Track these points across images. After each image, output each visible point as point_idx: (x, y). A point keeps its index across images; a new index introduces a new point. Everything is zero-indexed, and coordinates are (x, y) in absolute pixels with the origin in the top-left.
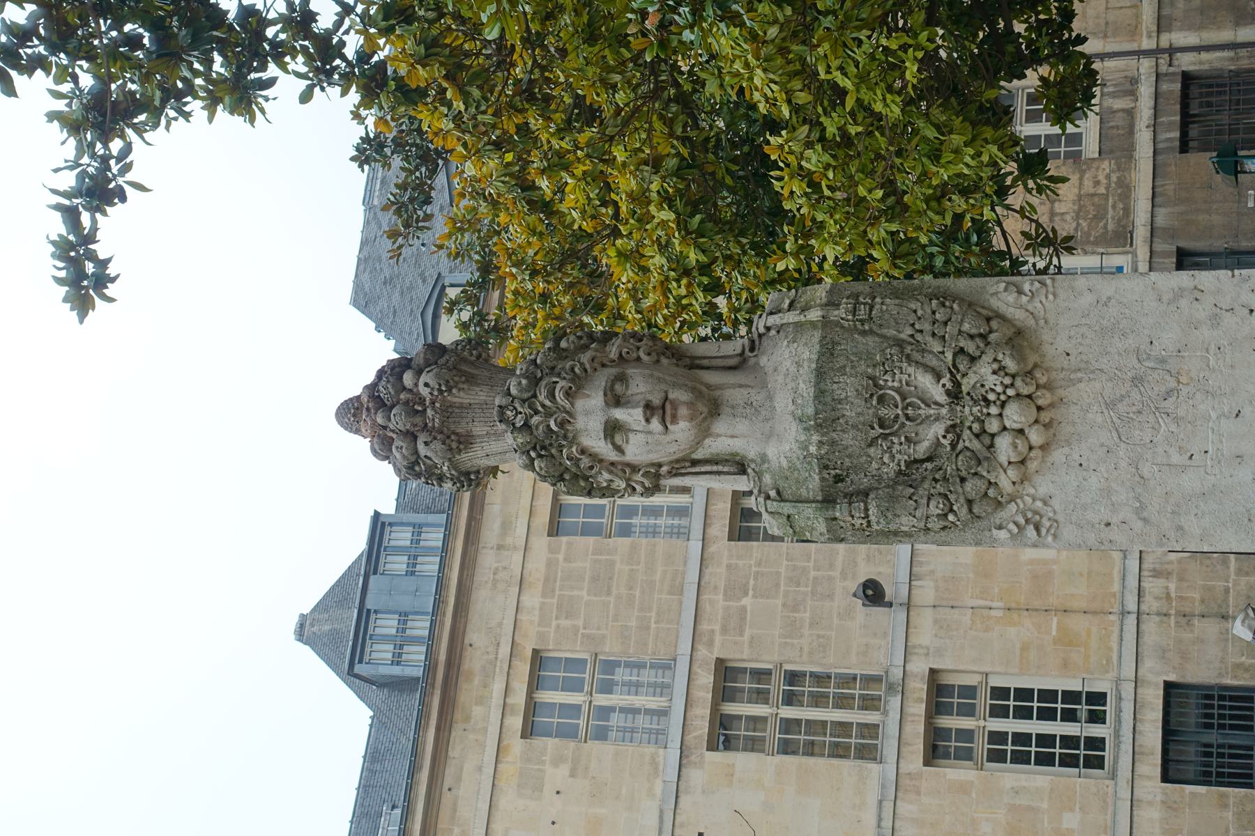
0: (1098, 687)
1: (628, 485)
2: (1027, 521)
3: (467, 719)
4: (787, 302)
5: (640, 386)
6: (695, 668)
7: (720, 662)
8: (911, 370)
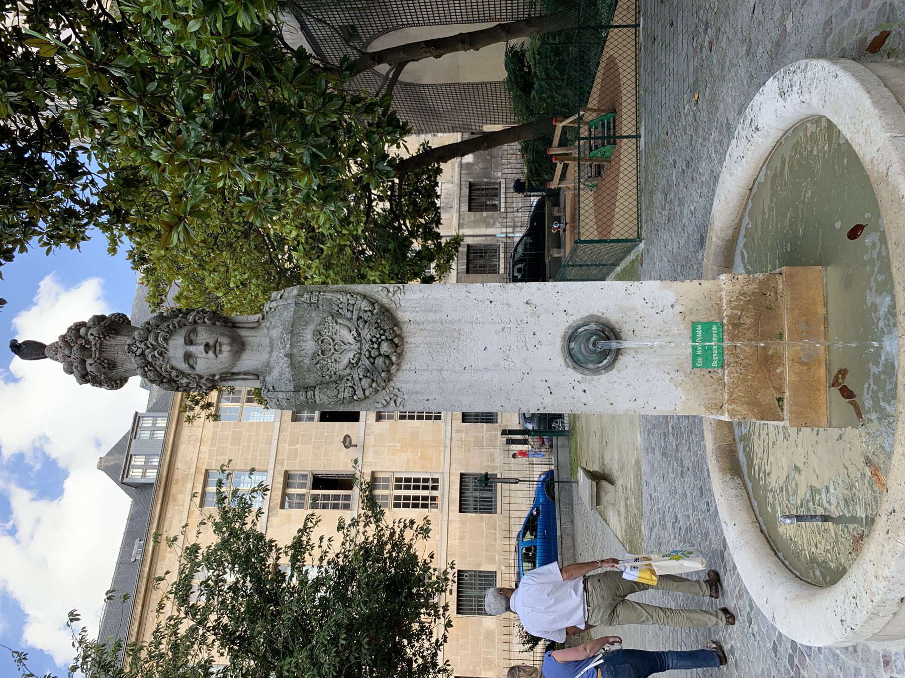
0: (435, 476)
1: (198, 385)
2: (391, 399)
3: (175, 500)
4: (280, 295)
5: (204, 336)
6: (275, 475)
7: (286, 472)
8: (337, 327)
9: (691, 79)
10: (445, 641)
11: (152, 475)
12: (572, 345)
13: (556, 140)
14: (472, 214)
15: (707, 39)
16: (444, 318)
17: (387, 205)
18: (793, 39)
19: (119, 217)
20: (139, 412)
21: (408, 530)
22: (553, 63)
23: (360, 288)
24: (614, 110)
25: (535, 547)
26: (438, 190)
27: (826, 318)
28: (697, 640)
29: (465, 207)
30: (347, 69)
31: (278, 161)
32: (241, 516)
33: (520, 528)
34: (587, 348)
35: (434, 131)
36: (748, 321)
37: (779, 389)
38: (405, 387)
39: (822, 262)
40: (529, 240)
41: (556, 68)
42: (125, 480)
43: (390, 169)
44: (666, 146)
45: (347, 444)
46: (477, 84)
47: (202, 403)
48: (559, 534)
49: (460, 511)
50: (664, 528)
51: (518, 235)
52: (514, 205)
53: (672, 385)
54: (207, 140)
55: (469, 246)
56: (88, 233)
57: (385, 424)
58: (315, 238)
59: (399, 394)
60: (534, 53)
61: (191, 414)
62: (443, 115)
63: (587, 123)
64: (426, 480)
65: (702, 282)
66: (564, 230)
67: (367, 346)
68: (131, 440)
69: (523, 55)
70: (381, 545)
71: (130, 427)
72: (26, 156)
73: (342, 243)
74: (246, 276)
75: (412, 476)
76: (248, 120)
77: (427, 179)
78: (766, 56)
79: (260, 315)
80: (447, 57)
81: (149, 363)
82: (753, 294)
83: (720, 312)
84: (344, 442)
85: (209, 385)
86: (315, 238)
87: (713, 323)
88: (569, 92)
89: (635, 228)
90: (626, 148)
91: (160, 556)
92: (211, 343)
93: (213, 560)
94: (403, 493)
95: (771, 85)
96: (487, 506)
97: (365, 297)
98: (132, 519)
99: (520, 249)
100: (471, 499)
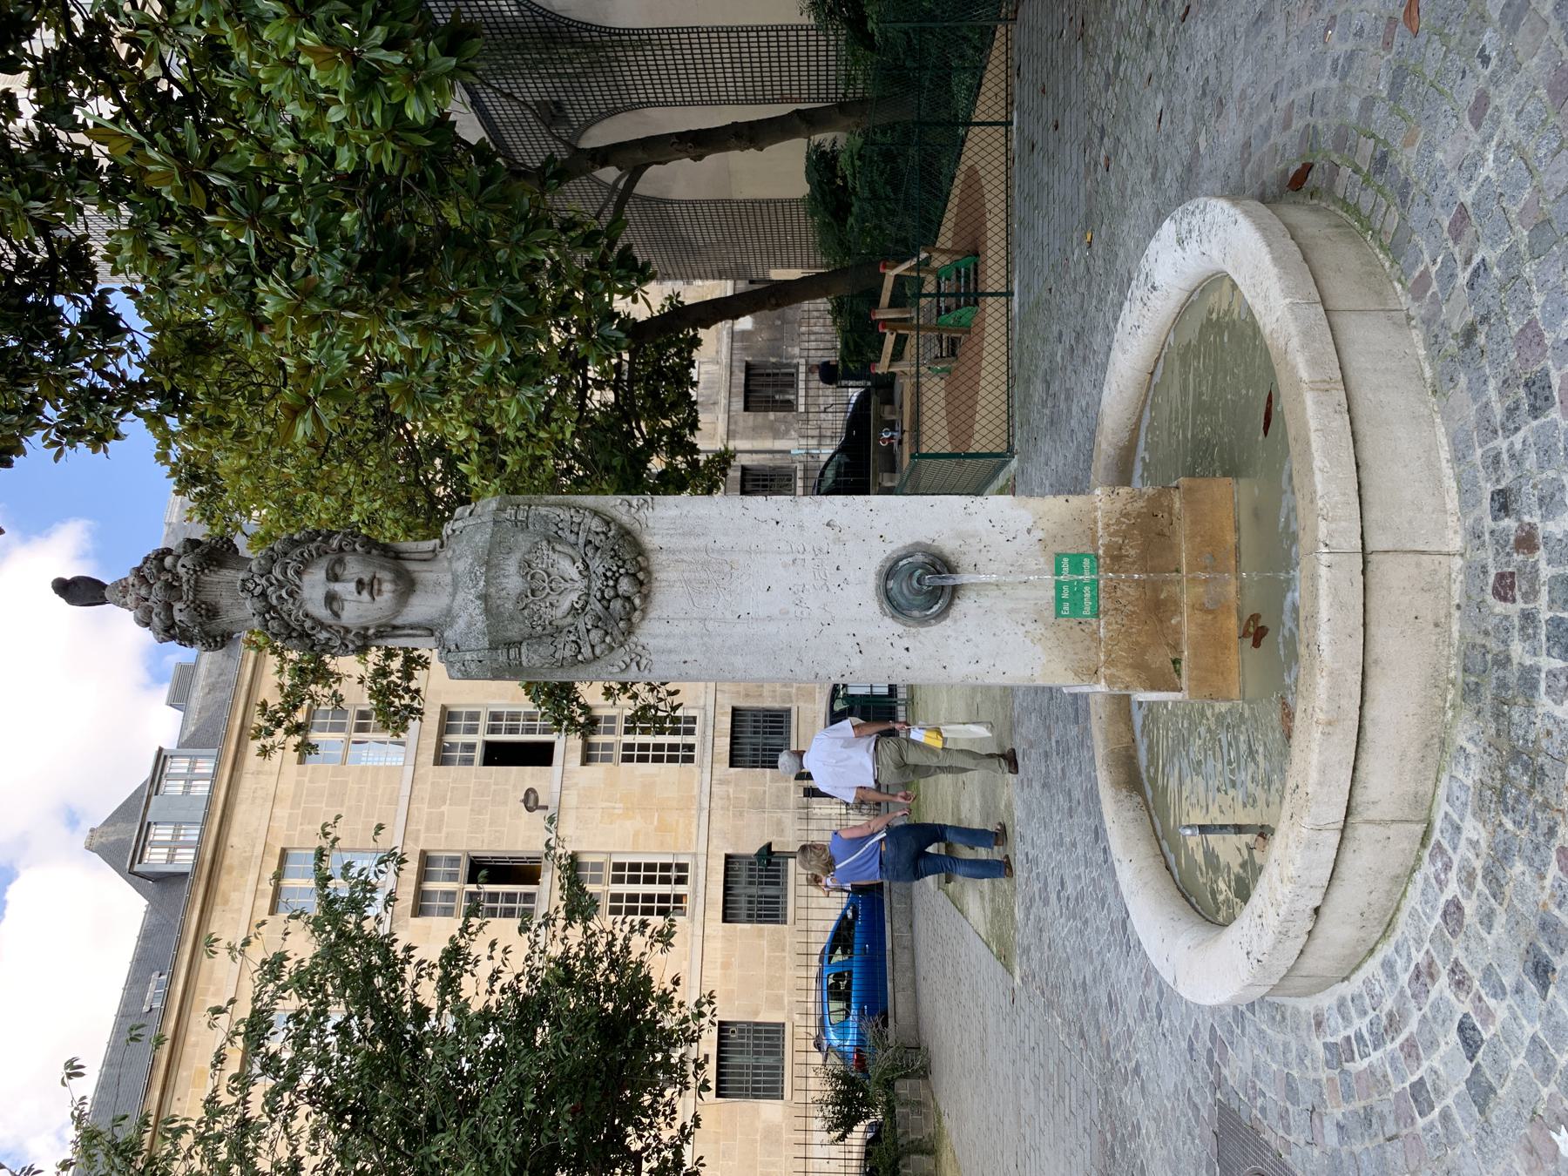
0: (681, 861)
3: (226, 902)
5: (354, 568)
8: (555, 556)
9: (1083, 210)
10: (697, 1125)
11: (185, 858)
12: (891, 584)
13: (885, 298)
14: (750, 416)
15: (1103, 153)
16: (711, 544)
17: (610, 396)
18: (1207, 164)
19: (175, 402)
20: (165, 747)
21: (636, 936)
22: (882, 174)
23: (590, 500)
24: (974, 253)
25: (850, 973)
26: (694, 373)
27: (1237, 548)
28: (1091, 1068)
29: (738, 404)
30: (553, 176)
31: (450, 318)
32: (356, 905)
33: (826, 938)
34: (910, 586)
35: (688, 277)
36: (1132, 552)
37: (1176, 647)
38: (652, 643)
39: (1233, 471)
40: (844, 459)
41: (887, 182)
42: (137, 868)
43: (621, 335)
44: (1049, 310)
45: (531, 804)
46: (760, 202)
47: (286, 724)
48: (889, 946)
49: (725, 920)
50: (1046, 902)
51: (826, 452)
52: (821, 400)
53: (1028, 641)
54: (350, 283)
55: (744, 469)
56: (123, 427)
57: (597, 770)
58: (492, 442)
59: (643, 653)
60: (851, 156)
61: (268, 742)
62: (703, 250)
63: (934, 271)
64: (666, 867)
65: (1070, 498)
66: (900, 442)
67: (599, 584)
68: (149, 797)
69: (835, 158)
70: (591, 961)
71: (147, 774)
72: (30, 299)
73: (538, 453)
74: (377, 505)
75: (643, 860)
76: (412, 254)
77: (677, 354)
78: (1175, 185)
79: (437, 541)
80: (712, 160)
81: (272, 607)
82: (1139, 515)
83: (1094, 540)
84: (525, 801)
85: (359, 643)
86: (492, 442)
87: (1084, 555)
88: (908, 221)
89: (1005, 436)
90: (992, 309)
91: (196, 1001)
92: (366, 579)
93: (304, 982)
94: (626, 889)
95: (1168, 228)
96: (770, 911)
97: (596, 513)
98: (147, 936)
99: (830, 474)
100: (744, 899)
